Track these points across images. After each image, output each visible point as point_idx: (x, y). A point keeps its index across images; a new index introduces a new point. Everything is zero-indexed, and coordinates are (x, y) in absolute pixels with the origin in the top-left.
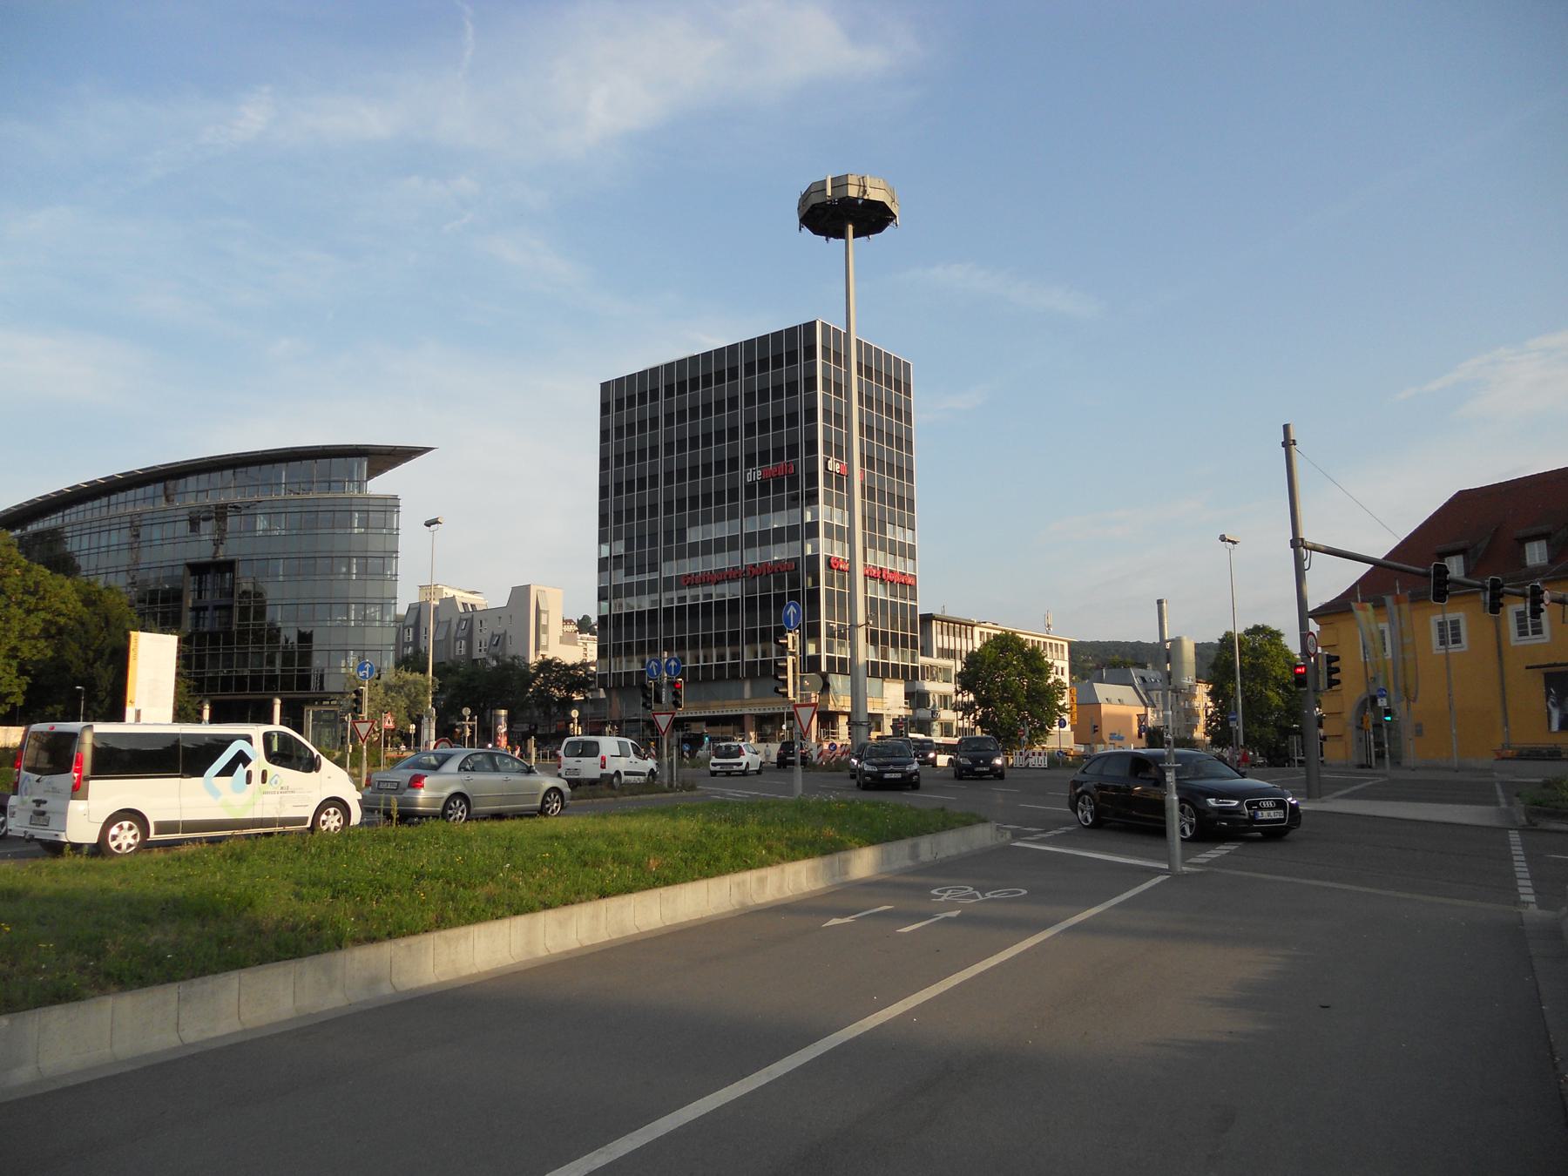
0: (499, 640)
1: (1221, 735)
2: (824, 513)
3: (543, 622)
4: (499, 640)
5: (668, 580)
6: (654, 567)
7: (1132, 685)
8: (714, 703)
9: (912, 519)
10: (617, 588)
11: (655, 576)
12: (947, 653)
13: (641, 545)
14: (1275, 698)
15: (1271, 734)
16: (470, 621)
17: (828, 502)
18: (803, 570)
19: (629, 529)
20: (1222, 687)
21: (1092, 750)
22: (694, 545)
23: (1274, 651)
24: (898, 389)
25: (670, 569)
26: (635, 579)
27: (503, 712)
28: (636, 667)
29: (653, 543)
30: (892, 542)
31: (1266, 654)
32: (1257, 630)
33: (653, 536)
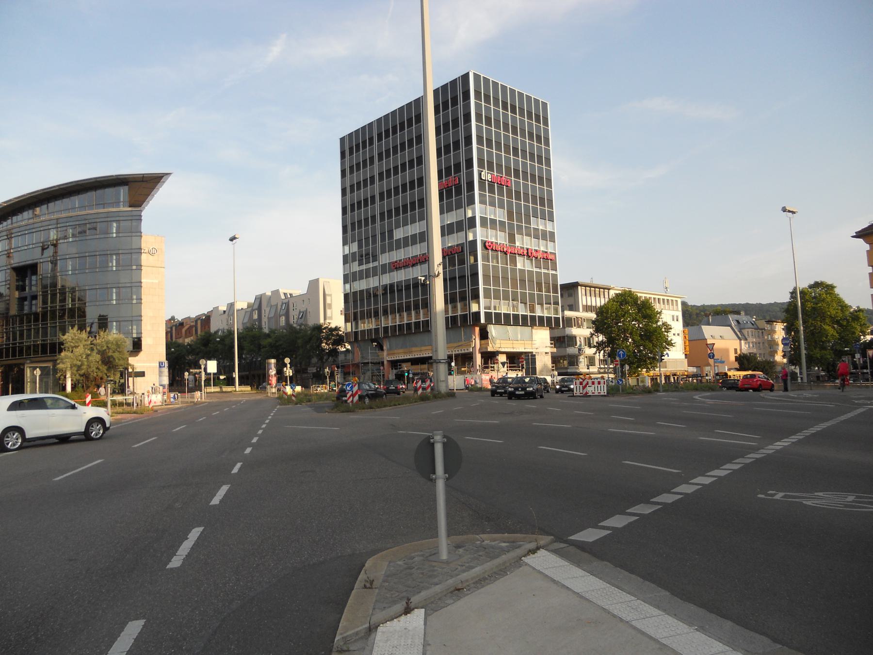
0: (304, 315)
1: (794, 359)
2: (478, 210)
3: (328, 301)
4: (304, 315)
5: (384, 266)
6: (375, 259)
7: (730, 326)
8: (414, 349)
9: (551, 214)
10: (354, 273)
11: (376, 264)
12: (587, 308)
13: (367, 244)
14: (831, 331)
15: (829, 356)
16: (287, 304)
17: (483, 202)
18: (467, 250)
19: (360, 234)
20: (792, 325)
21: (702, 371)
22: (398, 241)
23: (829, 299)
24: (538, 120)
25: (385, 259)
26: (364, 267)
27: (273, 361)
28: (372, 326)
29: (374, 242)
30: (536, 230)
31: (823, 300)
32: (817, 285)
33: (374, 236)
